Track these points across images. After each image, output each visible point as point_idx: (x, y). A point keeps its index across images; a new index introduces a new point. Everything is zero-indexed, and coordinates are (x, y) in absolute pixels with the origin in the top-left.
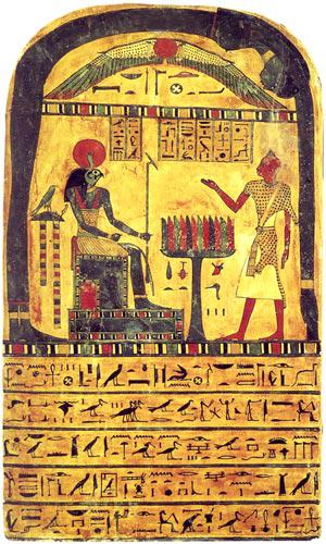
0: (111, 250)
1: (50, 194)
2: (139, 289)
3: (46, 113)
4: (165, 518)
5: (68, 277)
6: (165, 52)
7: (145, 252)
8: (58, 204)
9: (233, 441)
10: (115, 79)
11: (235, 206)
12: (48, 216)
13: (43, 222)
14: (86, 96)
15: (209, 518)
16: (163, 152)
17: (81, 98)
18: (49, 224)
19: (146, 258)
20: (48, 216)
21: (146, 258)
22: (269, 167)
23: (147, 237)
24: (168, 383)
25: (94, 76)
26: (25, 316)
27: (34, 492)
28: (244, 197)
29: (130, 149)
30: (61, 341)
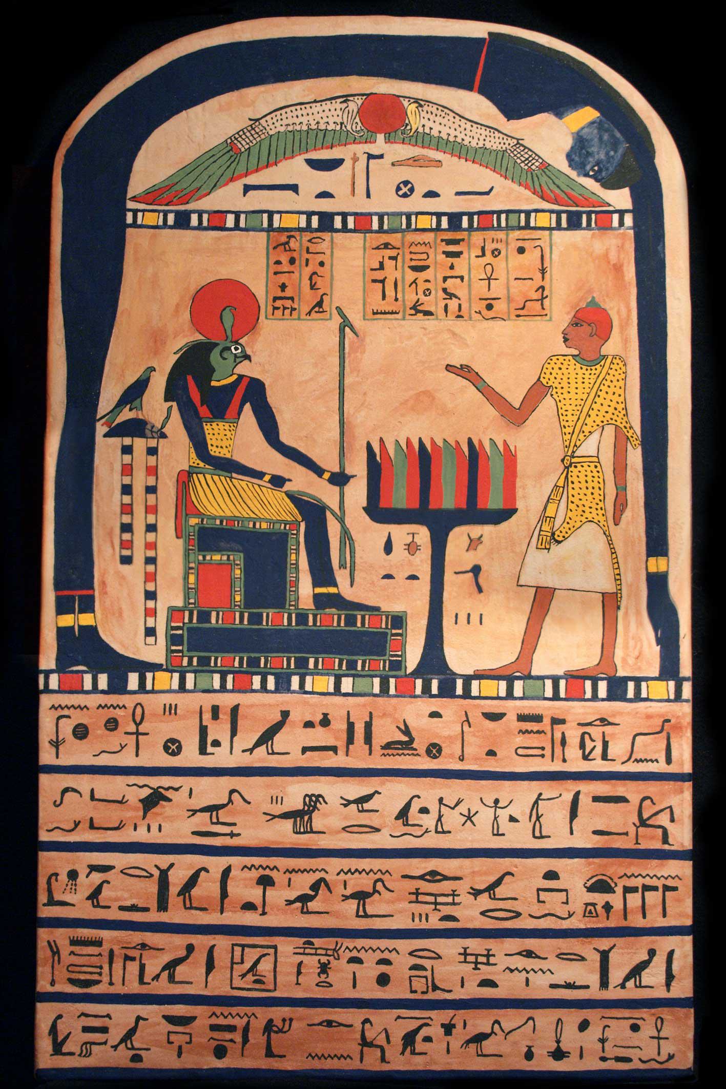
0: (266, 508)
1: (135, 392)
2: (322, 573)
3: (135, 225)
4: (370, 1035)
5: (172, 550)
6: (384, 118)
7: (335, 507)
8: (155, 406)
9: (498, 882)
10: (294, 169)
11: (516, 415)
12: (137, 428)
13: (127, 441)
14: (228, 197)
15: (448, 1029)
16: (376, 302)
17: (208, 203)
18: (140, 444)
19: (341, 520)
20: (137, 428)
21: (341, 520)
22: (589, 324)
23: (340, 479)
24: (240, 1023)
25: (232, 159)
26: (86, 619)
27: (96, 977)
28: (538, 391)
29: (308, 298)
30: (155, 667)
